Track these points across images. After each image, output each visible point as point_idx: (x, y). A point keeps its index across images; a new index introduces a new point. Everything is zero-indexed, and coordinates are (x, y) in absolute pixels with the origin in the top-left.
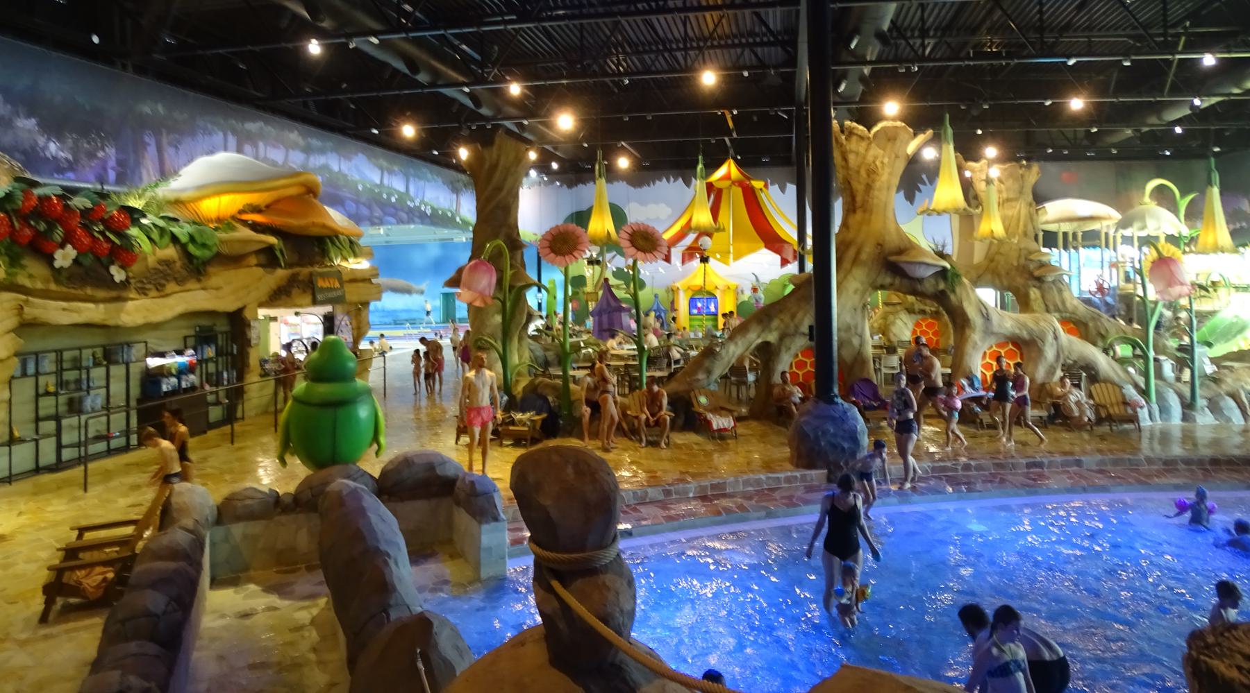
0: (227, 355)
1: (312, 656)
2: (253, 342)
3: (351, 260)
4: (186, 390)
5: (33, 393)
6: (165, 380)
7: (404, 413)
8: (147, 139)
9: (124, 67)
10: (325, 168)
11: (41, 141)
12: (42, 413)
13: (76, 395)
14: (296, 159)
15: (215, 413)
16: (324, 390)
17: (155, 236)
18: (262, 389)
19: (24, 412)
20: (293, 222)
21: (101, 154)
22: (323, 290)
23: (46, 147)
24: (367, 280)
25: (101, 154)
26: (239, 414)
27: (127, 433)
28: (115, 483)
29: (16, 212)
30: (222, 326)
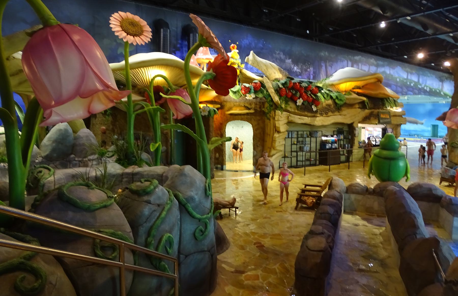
0: (347, 139)
1: (381, 245)
2: (356, 135)
3: (394, 108)
4: (334, 149)
5: (290, 143)
6: (327, 144)
7: (416, 170)
8: (322, 64)
9: (316, 40)
10: (384, 72)
11: (292, 66)
12: (293, 150)
13: (302, 145)
14: (373, 69)
15: (343, 158)
16: (385, 153)
17: (325, 96)
18: (358, 152)
19: (288, 149)
20: (372, 92)
21: (308, 70)
22: (383, 118)
23: (294, 68)
24: (400, 116)
25: (308, 70)
26: (351, 160)
27: (316, 160)
28: (312, 174)
29: (287, 87)
30: (346, 129)
